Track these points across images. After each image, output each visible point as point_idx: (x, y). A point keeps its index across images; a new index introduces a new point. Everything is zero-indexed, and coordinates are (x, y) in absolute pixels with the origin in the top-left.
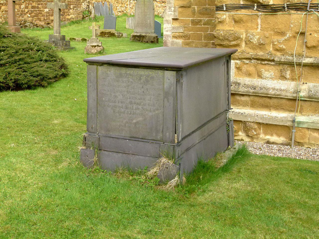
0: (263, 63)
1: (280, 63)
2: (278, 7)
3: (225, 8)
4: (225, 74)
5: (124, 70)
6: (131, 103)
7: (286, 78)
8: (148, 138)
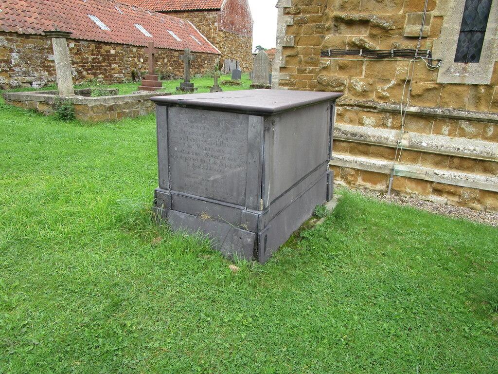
0: (365, 110)
1: (383, 111)
2: (384, 53)
3: (330, 53)
4: (265, 243)
5: (199, 113)
6: (207, 155)
7: (387, 127)
8: (228, 201)
